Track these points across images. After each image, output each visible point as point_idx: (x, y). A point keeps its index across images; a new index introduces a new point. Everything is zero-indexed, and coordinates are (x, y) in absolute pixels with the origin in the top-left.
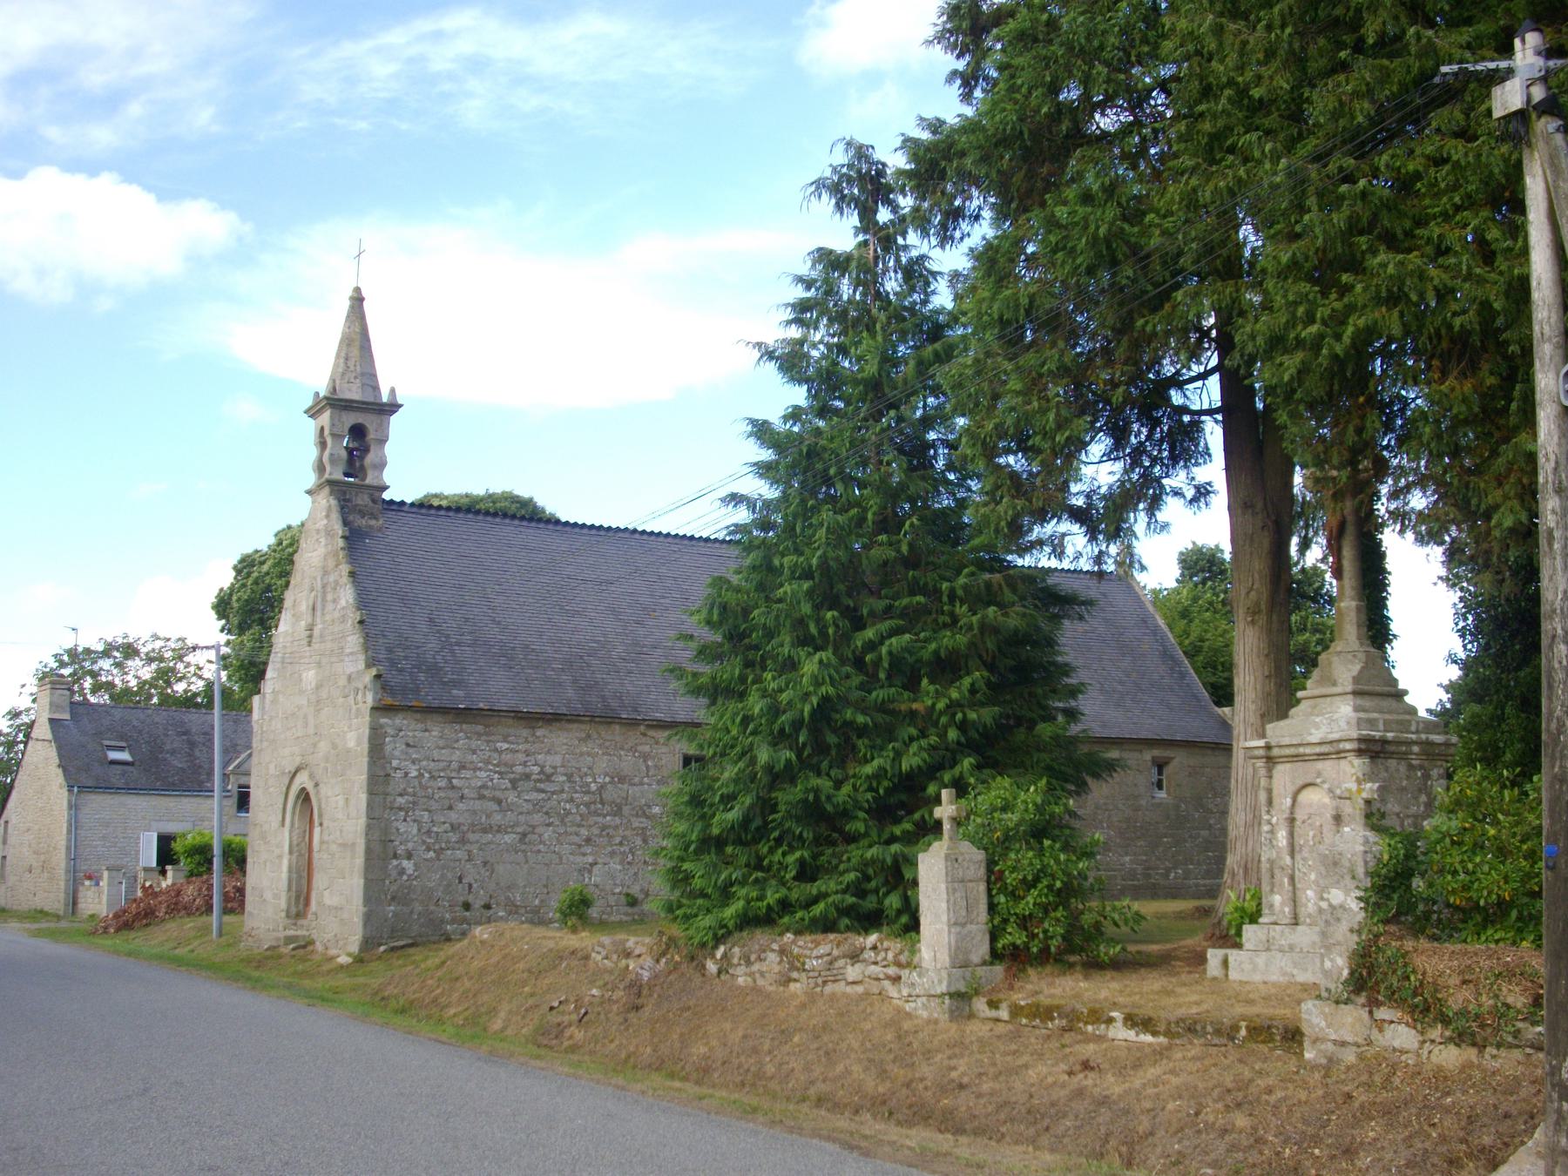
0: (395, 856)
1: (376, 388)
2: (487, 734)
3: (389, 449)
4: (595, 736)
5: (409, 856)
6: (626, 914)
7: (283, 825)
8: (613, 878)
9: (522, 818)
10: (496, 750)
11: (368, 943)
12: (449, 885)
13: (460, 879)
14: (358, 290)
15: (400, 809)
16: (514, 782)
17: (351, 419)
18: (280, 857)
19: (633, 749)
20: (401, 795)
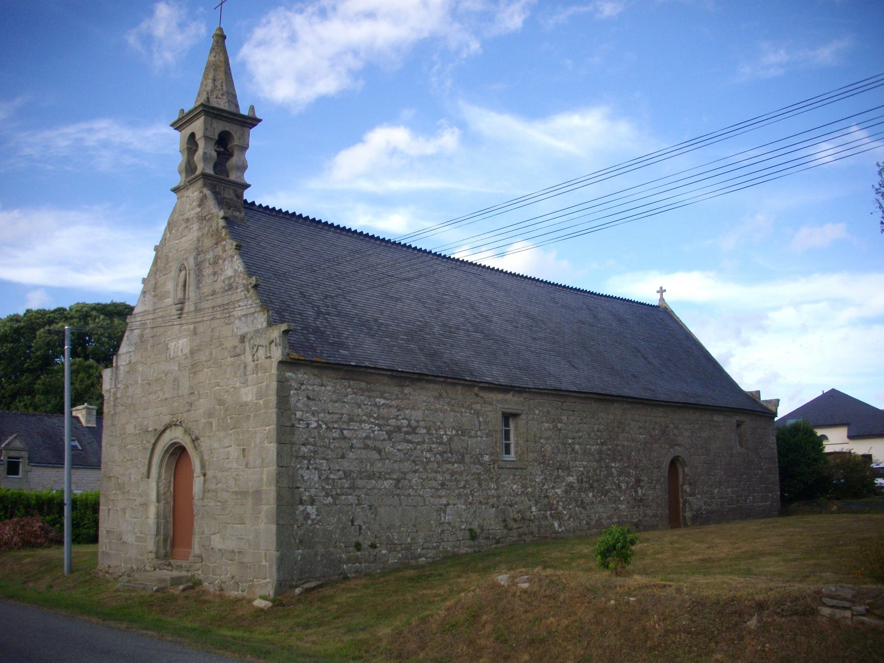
0: (301, 502)
1: (237, 106)
2: (369, 390)
3: (249, 155)
4: (445, 395)
5: (312, 503)
6: (470, 547)
7: (148, 477)
8: (460, 516)
9: (396, 466)
10: (375, 405)
11: (282, 587)
12: (344, 528)
13: (352, 521)
14: (221, 29)
15: (304, 457)
16: (389, 433)
17: (220, 126)
18: (145, 505)
19: (470, 408)
20: (304, 445)
